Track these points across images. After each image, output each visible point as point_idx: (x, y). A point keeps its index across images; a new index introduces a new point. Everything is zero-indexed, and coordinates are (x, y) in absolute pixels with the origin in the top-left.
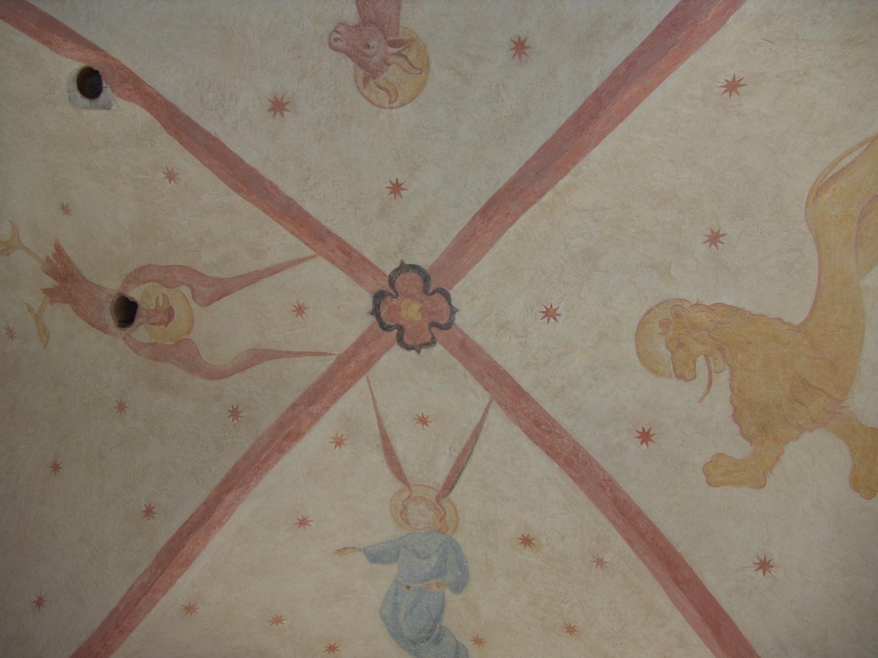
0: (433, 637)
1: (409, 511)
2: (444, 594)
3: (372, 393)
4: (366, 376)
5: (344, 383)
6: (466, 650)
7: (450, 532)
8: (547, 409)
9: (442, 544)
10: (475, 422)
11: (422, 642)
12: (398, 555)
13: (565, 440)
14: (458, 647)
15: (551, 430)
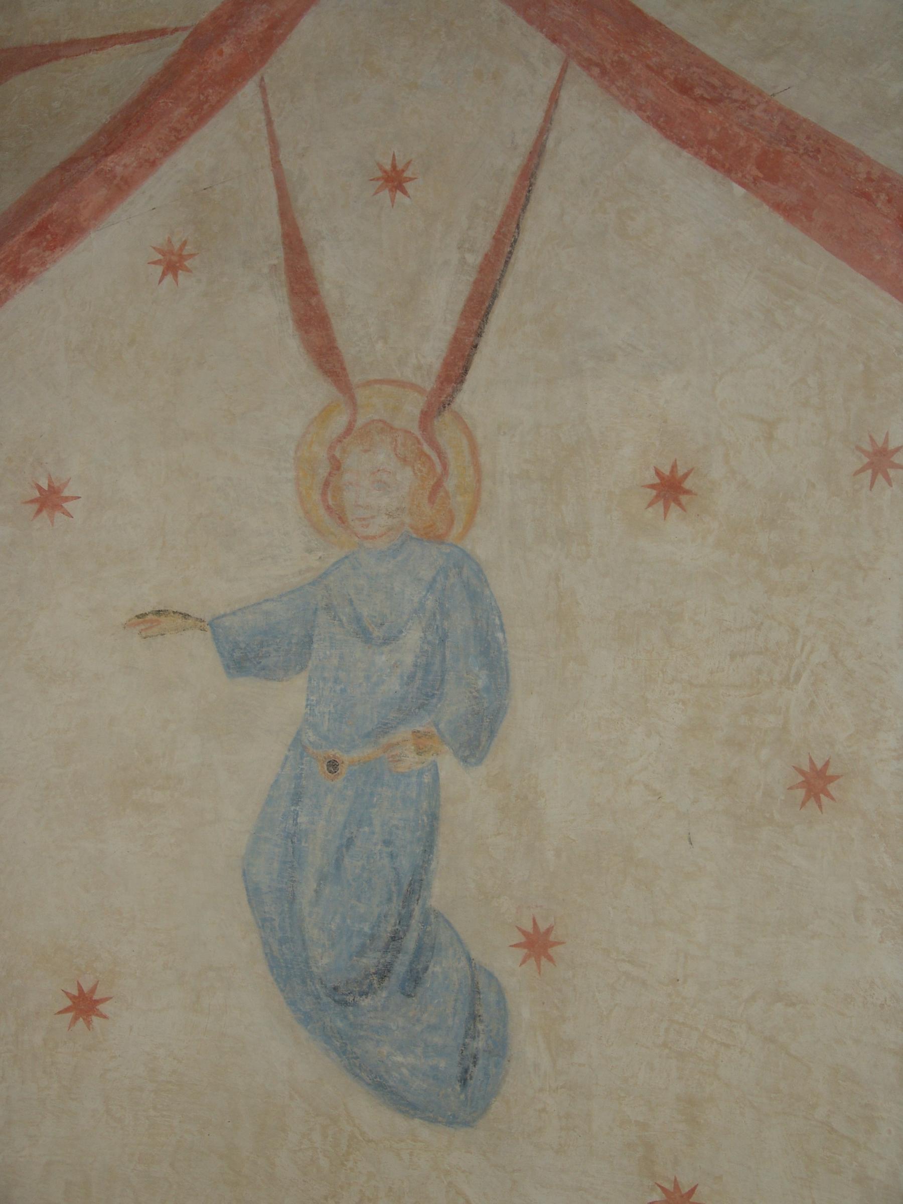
0: (400, 968)
1: (347, 477)
2: (436, 777)
3: (270, 123)
4: (256, 78)
5: (202, 97)
6: (500, 992)
7: (457, 529)
8: (710, 51)
9: (434, 580)
10: (525, 142)
11: (366, 994)
12: (308, 642)
13: (757, 112)
14: (475, 991)
15: (721, 94)
